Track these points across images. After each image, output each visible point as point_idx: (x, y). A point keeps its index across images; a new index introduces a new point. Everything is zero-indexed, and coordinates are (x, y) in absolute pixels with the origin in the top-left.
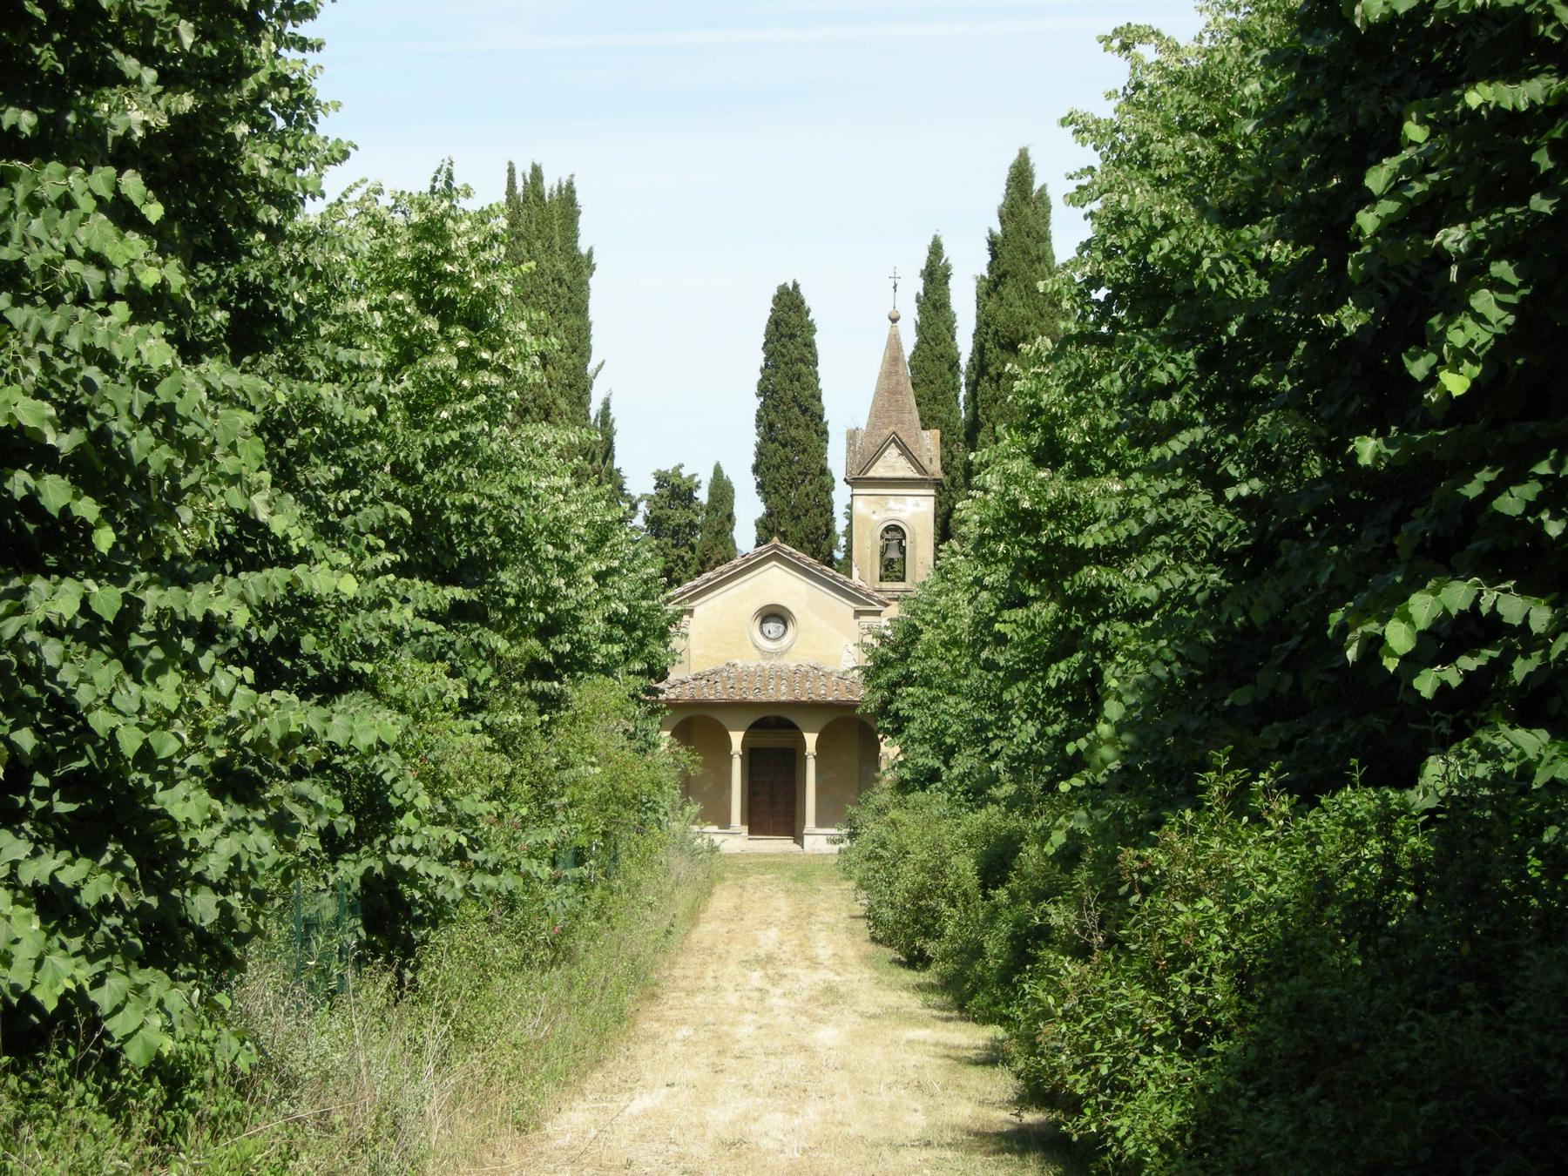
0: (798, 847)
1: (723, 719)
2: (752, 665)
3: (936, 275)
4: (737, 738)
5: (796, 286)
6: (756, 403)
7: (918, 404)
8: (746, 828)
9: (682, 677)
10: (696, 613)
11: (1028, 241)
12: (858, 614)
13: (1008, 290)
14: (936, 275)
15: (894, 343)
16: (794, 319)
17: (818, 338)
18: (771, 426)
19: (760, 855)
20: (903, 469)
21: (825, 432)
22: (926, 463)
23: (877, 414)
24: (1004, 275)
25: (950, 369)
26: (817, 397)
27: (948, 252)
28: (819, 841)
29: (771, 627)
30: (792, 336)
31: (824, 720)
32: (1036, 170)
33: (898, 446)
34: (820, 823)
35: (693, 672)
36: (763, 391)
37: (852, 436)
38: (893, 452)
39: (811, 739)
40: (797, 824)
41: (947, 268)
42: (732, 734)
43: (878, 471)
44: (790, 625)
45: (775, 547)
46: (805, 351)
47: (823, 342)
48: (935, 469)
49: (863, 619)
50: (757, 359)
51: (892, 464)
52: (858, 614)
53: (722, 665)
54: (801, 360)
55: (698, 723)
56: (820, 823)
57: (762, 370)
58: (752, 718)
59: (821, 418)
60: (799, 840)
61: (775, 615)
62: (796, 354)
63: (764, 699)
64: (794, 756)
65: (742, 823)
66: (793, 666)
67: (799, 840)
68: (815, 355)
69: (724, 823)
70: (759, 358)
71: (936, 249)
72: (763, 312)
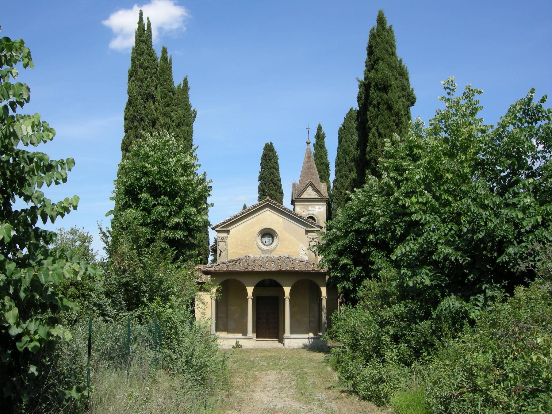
0: (280, 345)
1: (242, 280)
2: (258, 257)
3: (320, 137)
4: (250, 290)
5: (271, 144)
6: (258, 183)
7: (319, 172)
8: (255, 335)
9: (223, 261)
10: (231, 232)
11: (387, 46)
12: (307, 232)
13: (381, 65)
14: (320, 137)
15: (308, 150)
16: (271, 154)
17: (279, 162)
18: (263, 190)
19: (265, 350)
20: (314, 195)
21: (282, 193)
22: (322, 193)
23: (303, 176)
24: (377, 60)
25: (326, 168)
26: (279, 180)
27: (324, 130)
28: (296, 341)
29: (266, 239)
30: (270, 160)
31: (294, 280)
32: (387, 19)
33: (312, 187)
34: (292, 332)
35: (229, 260)
36: (260, 179)
37: (294, 185)
38: (310, 189)
39: (287, 290)
40: (280, 333)
41: (324, 134)
42: (247, 288)
43: (305, 196)
44: (275, 240)
45: (268, 201)
46: (275, 165)
47: (281, 163)
48: (326, 195)
49: (310, 234)
50: (258, 169)
51: (310, 193)
52: (307, 232)
53: (243, 257)
54: (273, 168)
55: (230, 284)
56: (292, 332)
57: (260, 172)
58: (257, 280)
59: (281, 188)
60: (281, 341)
61: (268, 234)
62: (272, 165)
63: (263, 269)
64: (279, 300)
65: (253, 332)
66: (277, 257)
67: (281, 341)
68: (278, 166)
69: (245, 333)
70: (259, 168)
71: (320, 128)
72: (260, 153)
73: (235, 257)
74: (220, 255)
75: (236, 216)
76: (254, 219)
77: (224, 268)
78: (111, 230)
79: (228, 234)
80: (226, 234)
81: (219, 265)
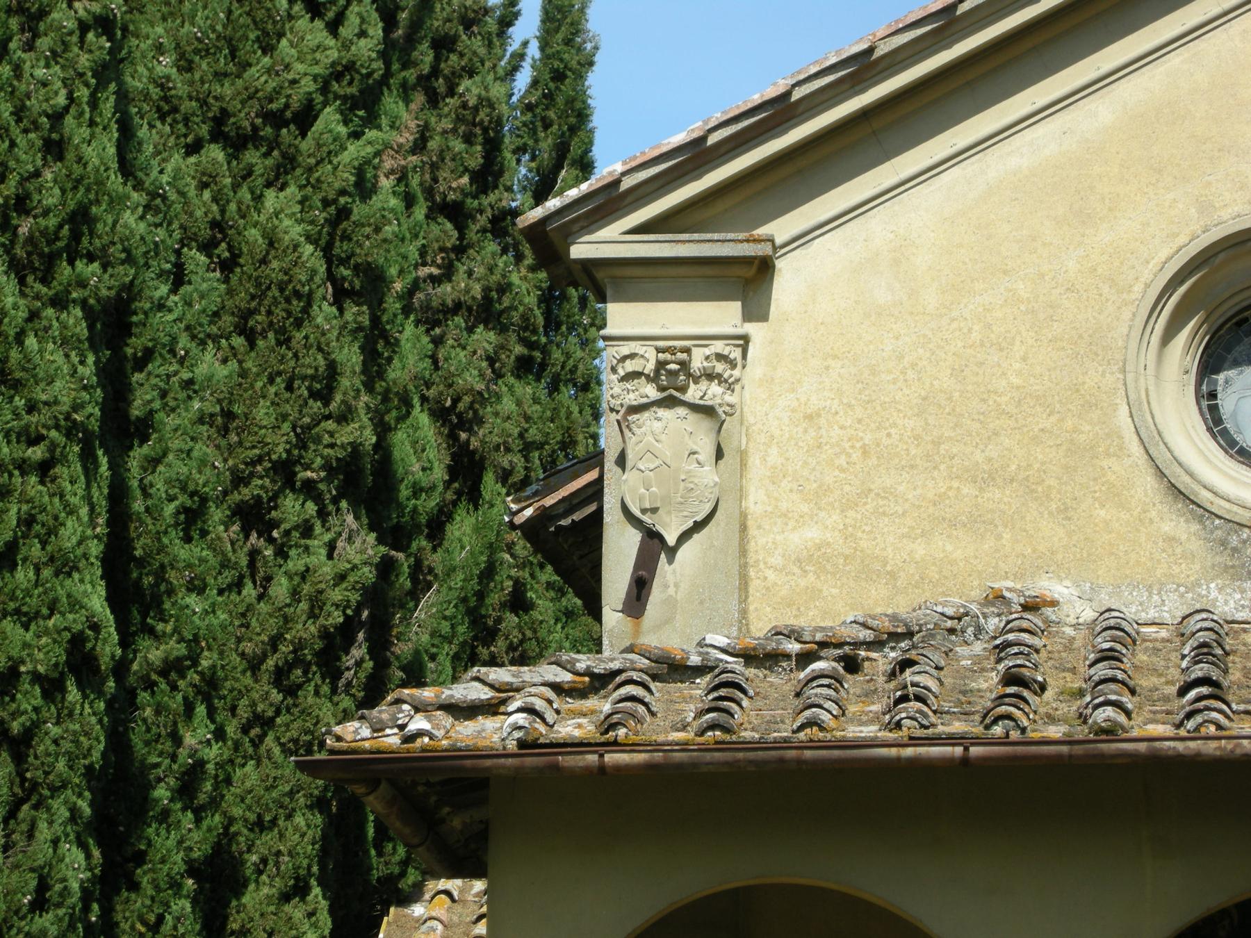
2: (1155, 608)
10: (790, 282)
35: (759, 628)
73: (834, 609)
74: (641, 587)
75: (863, 67)
76: (1099, 112)
77: (674, 720)
78: (386, 92)
79: (756, 311)
80: (721, 316)
81: (599, 682)
